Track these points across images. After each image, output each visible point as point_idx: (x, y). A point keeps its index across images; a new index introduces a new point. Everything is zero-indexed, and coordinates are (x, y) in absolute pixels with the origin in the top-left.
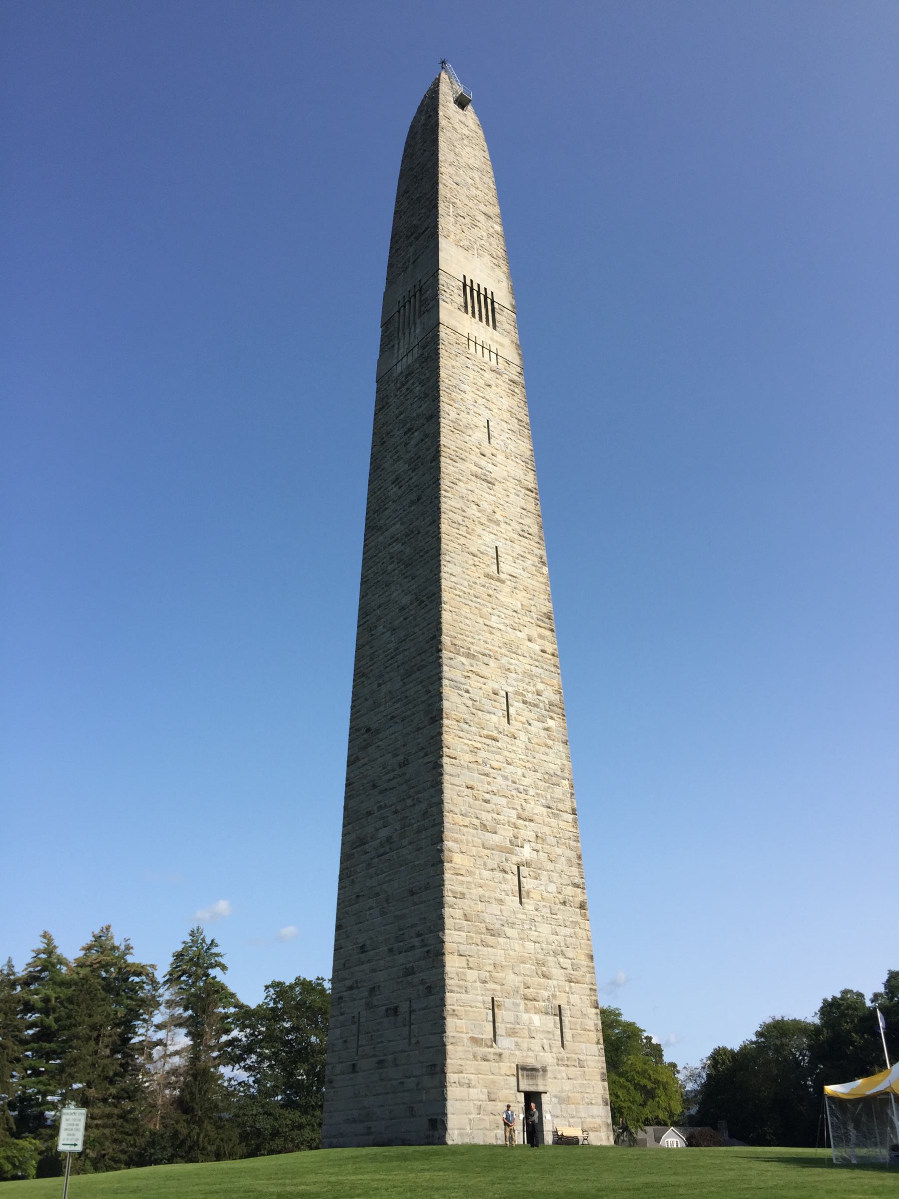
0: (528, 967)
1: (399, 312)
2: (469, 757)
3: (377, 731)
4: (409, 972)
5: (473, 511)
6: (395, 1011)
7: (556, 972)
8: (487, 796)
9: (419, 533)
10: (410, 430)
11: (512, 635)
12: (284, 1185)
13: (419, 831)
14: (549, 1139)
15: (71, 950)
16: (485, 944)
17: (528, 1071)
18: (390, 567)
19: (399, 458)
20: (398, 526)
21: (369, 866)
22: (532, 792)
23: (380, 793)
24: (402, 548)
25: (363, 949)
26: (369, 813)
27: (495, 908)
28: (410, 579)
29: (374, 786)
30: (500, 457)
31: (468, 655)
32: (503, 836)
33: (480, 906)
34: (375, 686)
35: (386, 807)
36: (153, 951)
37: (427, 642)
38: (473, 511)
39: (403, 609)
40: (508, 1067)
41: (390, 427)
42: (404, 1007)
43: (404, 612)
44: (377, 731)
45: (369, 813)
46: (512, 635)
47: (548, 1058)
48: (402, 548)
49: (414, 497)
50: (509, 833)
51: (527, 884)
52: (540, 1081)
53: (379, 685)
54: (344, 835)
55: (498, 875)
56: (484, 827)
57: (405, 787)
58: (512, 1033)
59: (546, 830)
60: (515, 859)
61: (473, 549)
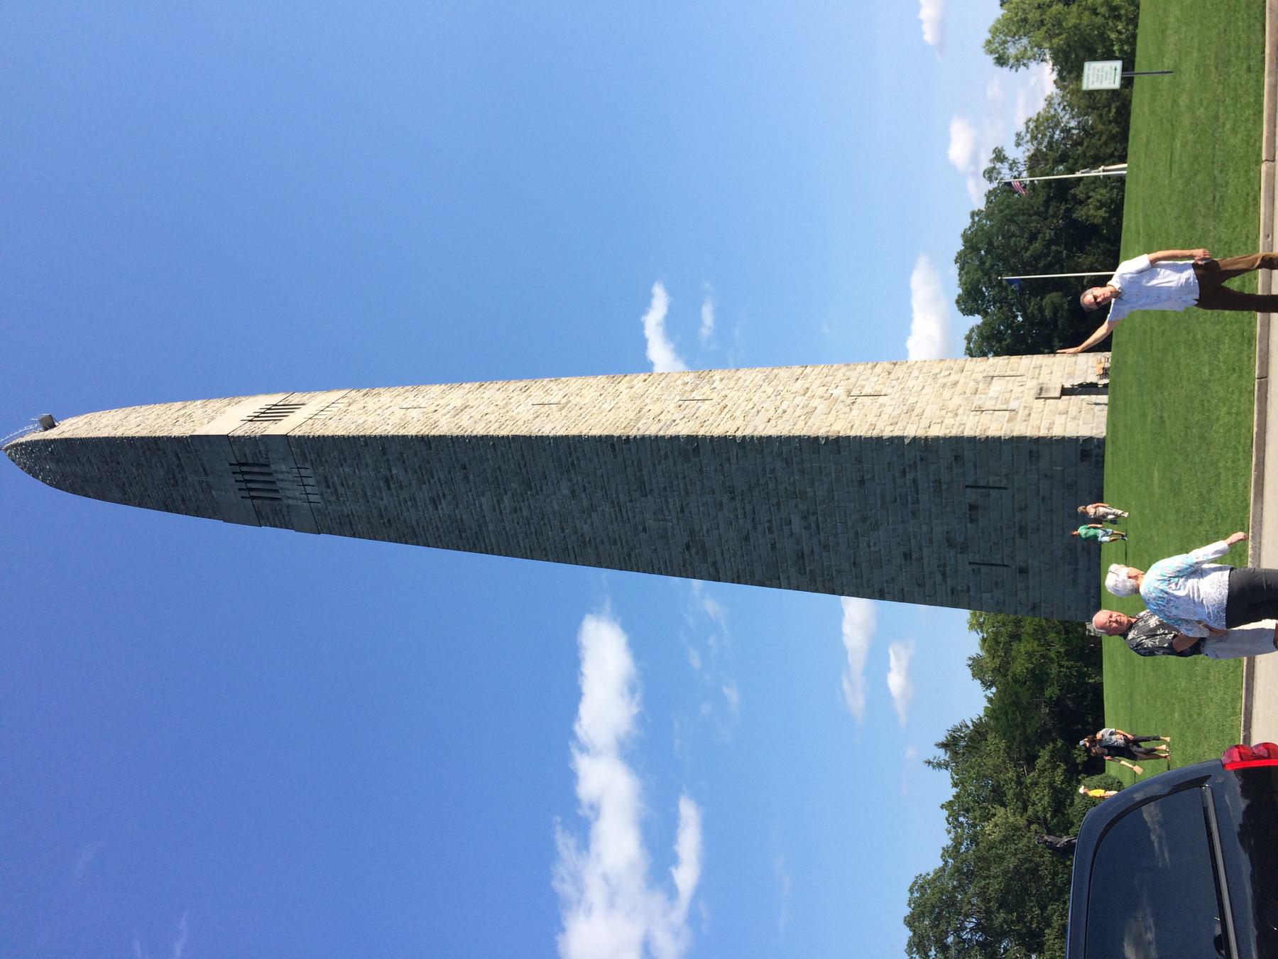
0: (947, 393)
1: (253, 498)
3: (692, 533)
6: (973, 507)
8: (780, 411)
9: (499, 468)
10: (387, 481)
13: (802, 472)
16: (921, 415)
17: (1041, 395)
18: (525, 513)
19: (413, 499)
20: (483, 500)
21: (826, 548)
22: (781, 388)
23: (755, 528)
24: (509, 493)
25: (907, 556)
26: (773, 546)
27: (888, 410)
28: (544, 482)
29: (747, 538)
30: (442, 402)
31: (638, 420)
33: (884, 417)
34: (644, 536)
35: (770, 521)
37: (615, 457)
39: (573, 492)
41: (374, 511)
42: (972, 496)
43: (577, 492)
44: (692, 533)
45: (773, 546)
48: (509, 493)
52: (1051, 385)
53: (644, 530)
55: (856, 406)
57: (756, 492)
58: (1007, 401)
59: (818, 382)
60: (843, 397)
61: (531, 417)
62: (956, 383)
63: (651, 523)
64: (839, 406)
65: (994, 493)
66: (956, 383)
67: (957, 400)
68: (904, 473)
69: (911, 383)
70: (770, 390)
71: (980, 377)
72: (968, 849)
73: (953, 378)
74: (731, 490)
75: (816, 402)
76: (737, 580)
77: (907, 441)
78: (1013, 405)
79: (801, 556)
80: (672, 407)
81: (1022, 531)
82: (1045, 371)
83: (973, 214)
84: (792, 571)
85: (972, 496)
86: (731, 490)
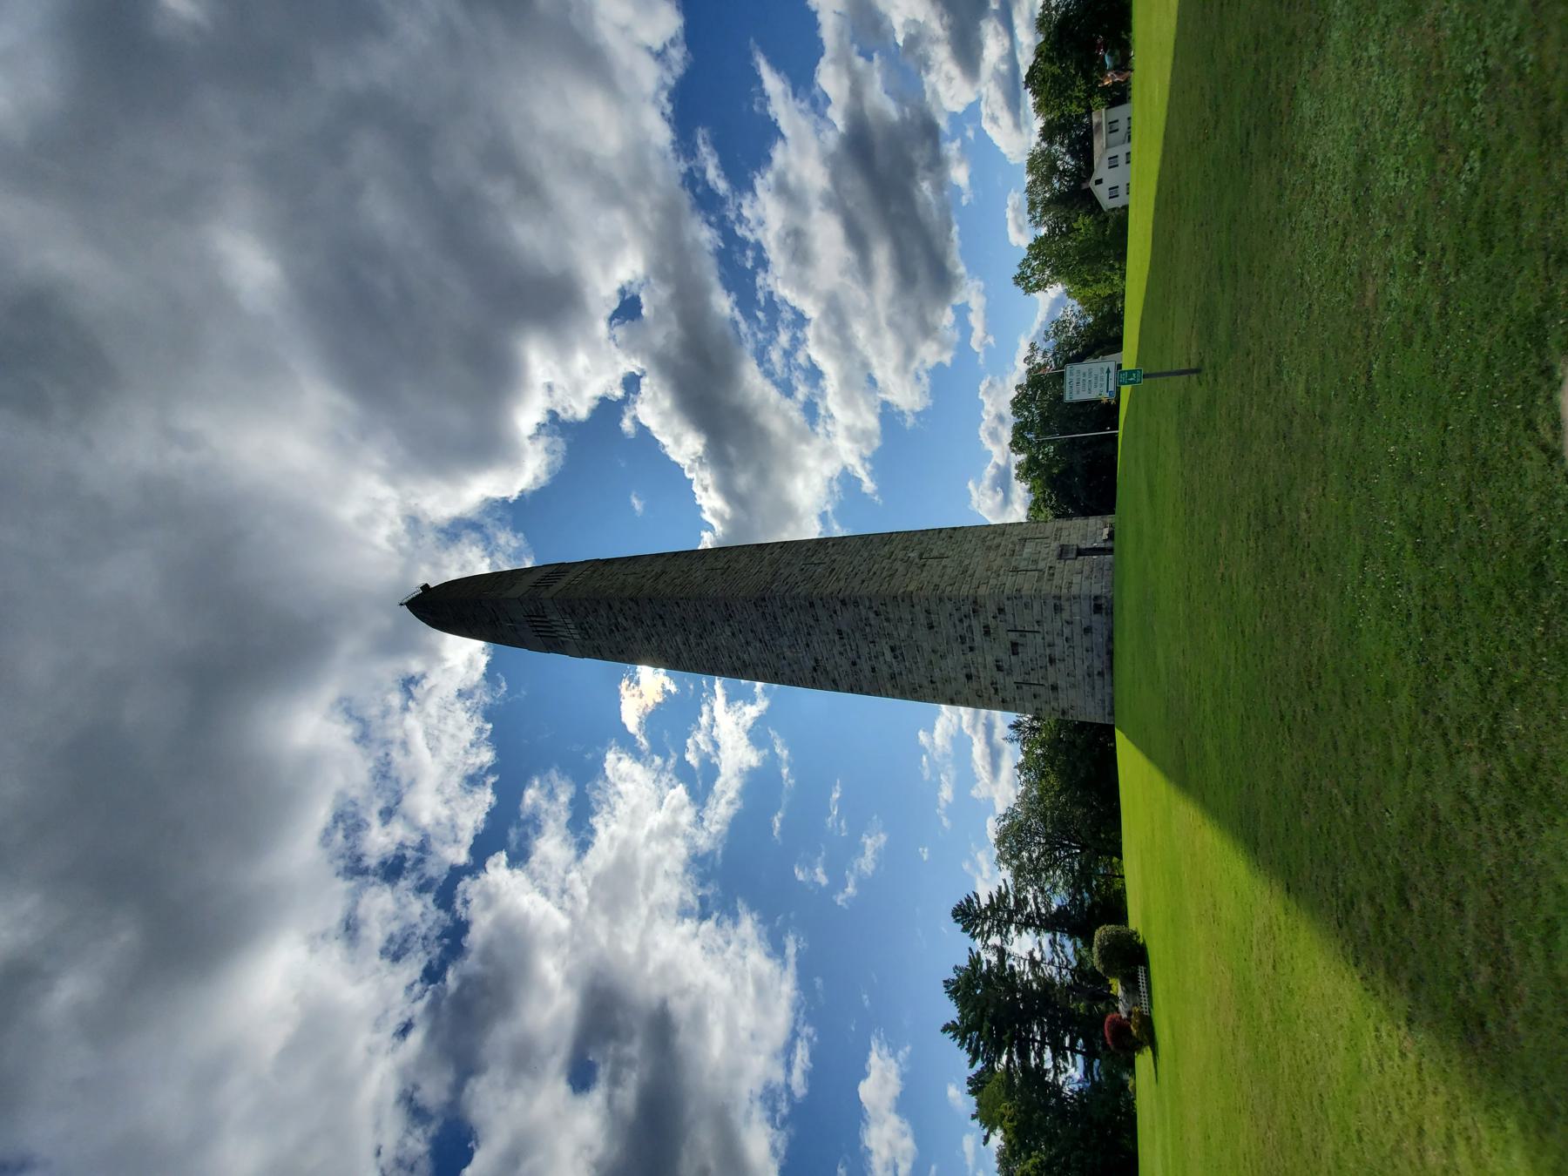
0: (992, 555)
2: (842, 583)
3: (816, 661)
4: (987, 631)
5: (677, 581)
7: (997, 541)
11: (766, 562)
12: (1153, 1128)
14: (1109, 544)
15: (952, 1012)
16: (972, 575)
17: (1063, 553)
21: (910, 671)
25: (969, 677)
26: (873, 670)
27: (949, 571)
29: (854, 664)
32: (900, 567)
36: (957, 949)
38: (677, 581)
40: (1059, 565)
42: (1013, 636)
44: (816, 661)
45: (873, 670)
46: (766, 562)
47: (1054, 545)
49: (659, 623)
50: (898, 565)
51: (935, 553)
54: (887, 696)
56: (892, 575)
58: (1035, 562)
62: (998, 546)
63: (788, 654)
64: (914, 568)
65: (1030, 635)
66: (998, 546)
67: (999, 561)
68: (961, 621)
69: (966, 546)
70: (866, 555)
71: (1016, 539)
72: (1040, 1055)
73: (997, 541)
74: (840, 632)
75: (898, 565)
76: (851, 690)
77: (1126, 1076)
78: (1041, 565)
79: (893, 677)
80: (796, 571)
81: (1052, 661)
82: (1065, 533)
83: (1018, 387)
84: (889, 686)
85: (1013, 636)
86: (840, 632)
